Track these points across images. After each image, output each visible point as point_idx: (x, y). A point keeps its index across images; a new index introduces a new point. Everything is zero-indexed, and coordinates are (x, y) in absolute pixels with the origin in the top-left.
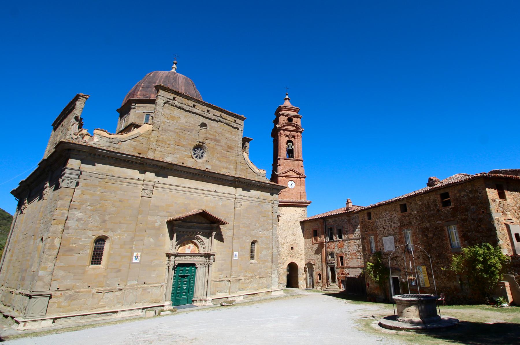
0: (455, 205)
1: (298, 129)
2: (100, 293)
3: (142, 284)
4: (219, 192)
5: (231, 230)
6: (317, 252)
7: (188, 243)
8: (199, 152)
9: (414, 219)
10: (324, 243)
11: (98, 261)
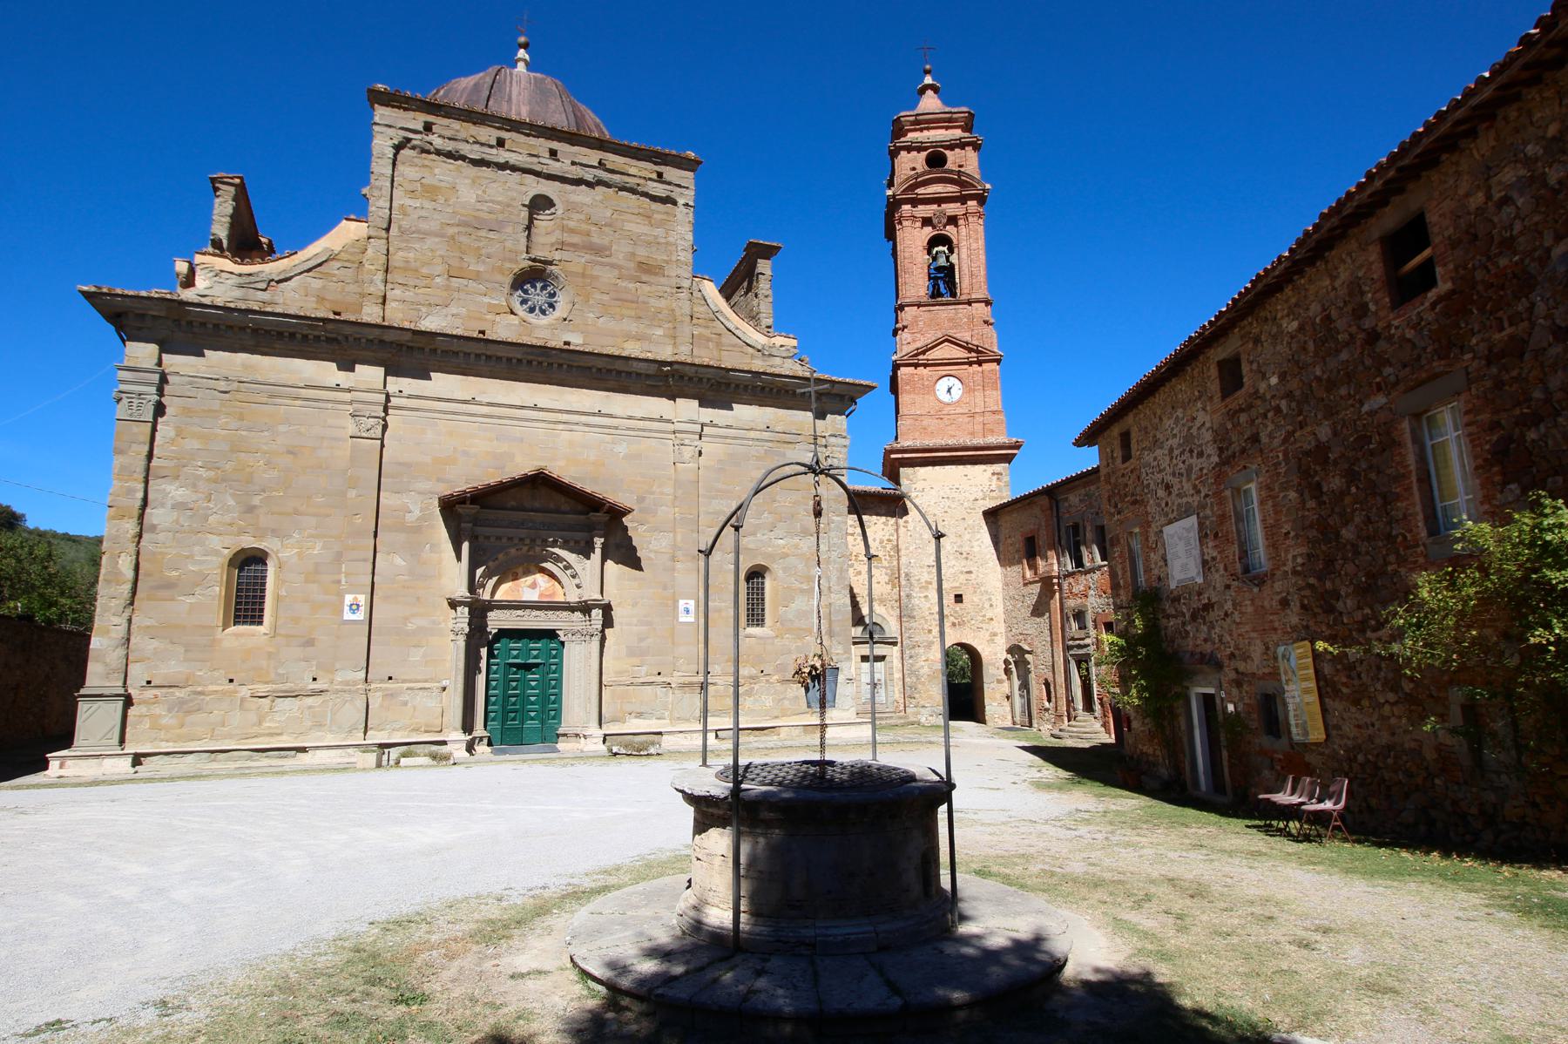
0: (1462, 272)
1: (966, 190)
3: (382, 681)
6: (1039, 609)
7: (527, 573)
9: (1270, 415)
11: (253, 617)
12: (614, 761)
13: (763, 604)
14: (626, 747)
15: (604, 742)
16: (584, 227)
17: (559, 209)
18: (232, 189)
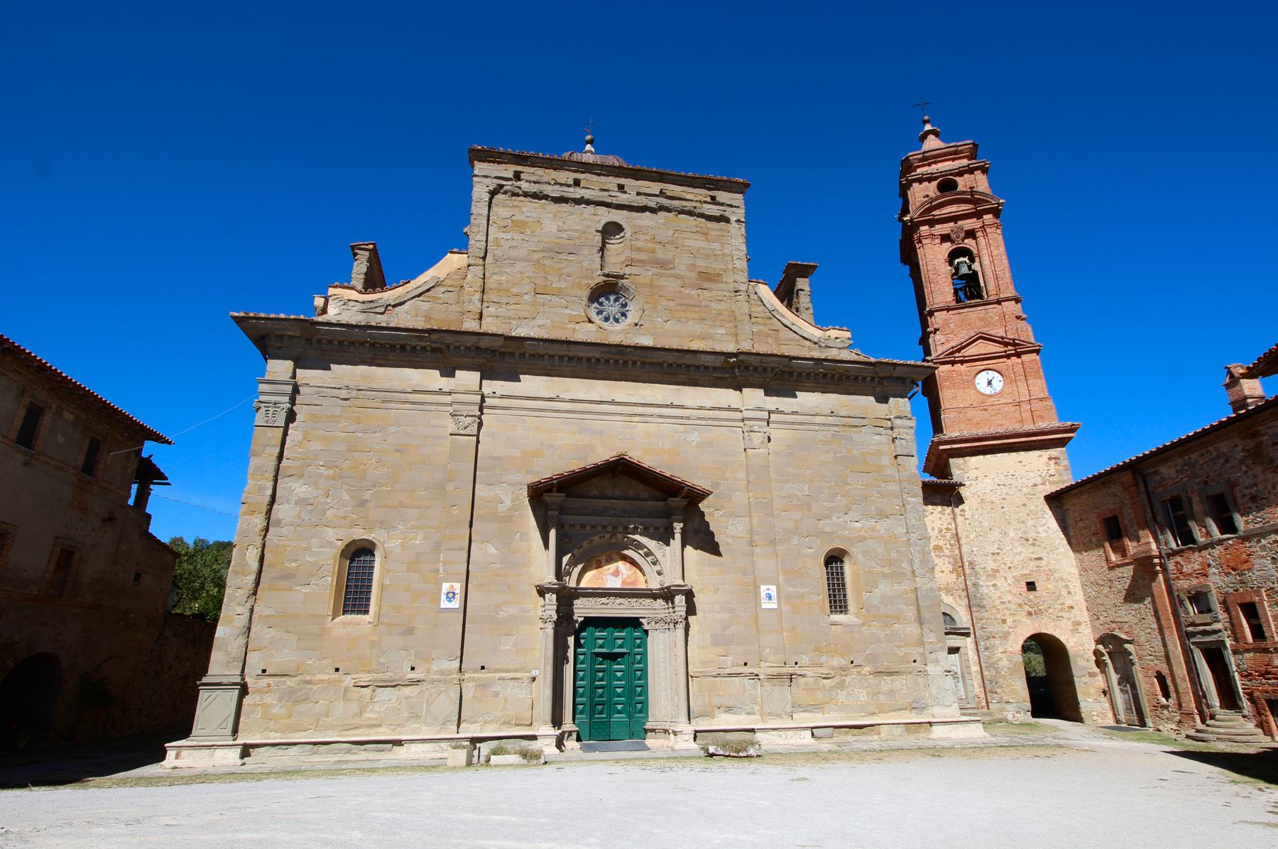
2: (362, 687)
3: (475, 671)
5: (743, 517)
6: (1134, 594)
7: (610, 560)
8: (612, 306)
10: (1156, 557)
12: (714, 764)
13: (844, 590)
14: (723, 746)
15: (695, 740)
16: (649, 245)
17: (628, 232)
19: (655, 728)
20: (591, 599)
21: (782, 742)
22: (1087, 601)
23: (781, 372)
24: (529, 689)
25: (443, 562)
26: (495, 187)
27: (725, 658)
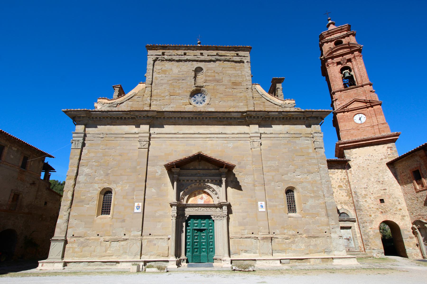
1: (352, 49)
3: (147, 236)
4: (225, 134)
7: (199, 193)
8: (199, 98)
11: (107, 212)
12: (233, 273)
13: (294, 203)
14: (239, 267)
16: (213, 74)
17: (204, 70)
18: (118, 89)
19: (217, 258)
20: (191, 208)
21: (267, 265)
22: (407, 206)
23: (265, 118)
24: (167, 243)
25: (135, 195)
26: (155, 58)
27: (244, 231)
